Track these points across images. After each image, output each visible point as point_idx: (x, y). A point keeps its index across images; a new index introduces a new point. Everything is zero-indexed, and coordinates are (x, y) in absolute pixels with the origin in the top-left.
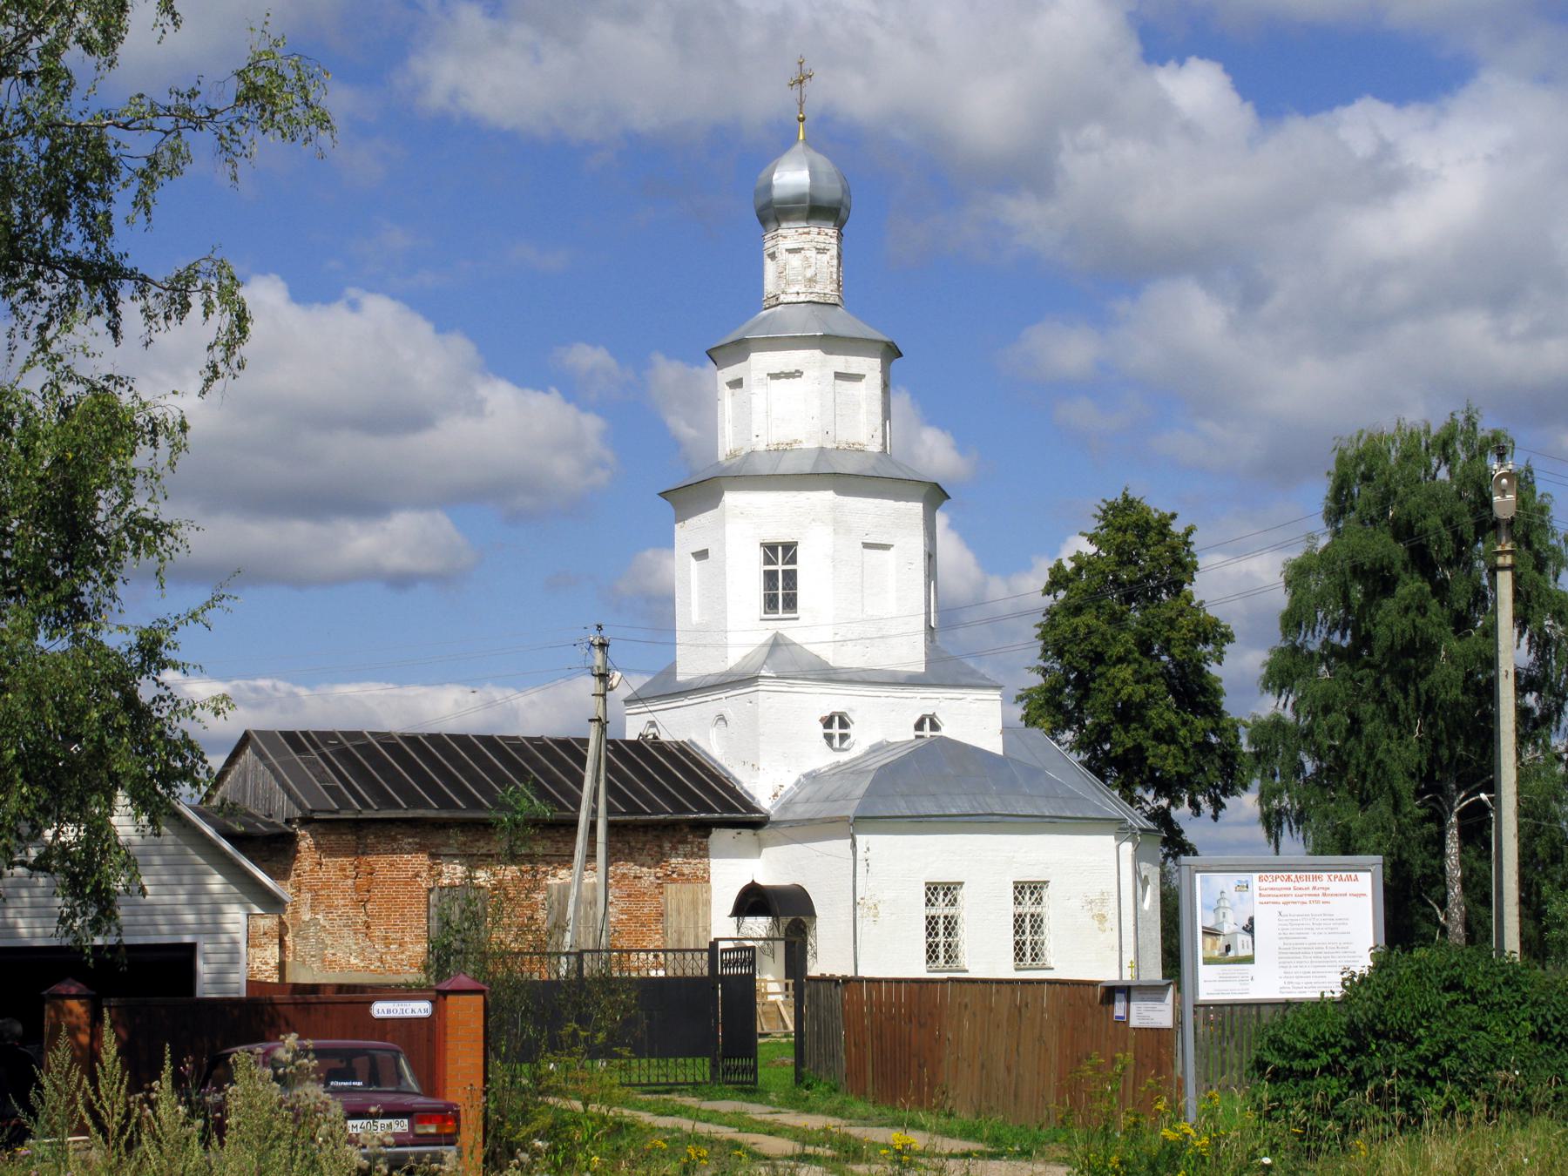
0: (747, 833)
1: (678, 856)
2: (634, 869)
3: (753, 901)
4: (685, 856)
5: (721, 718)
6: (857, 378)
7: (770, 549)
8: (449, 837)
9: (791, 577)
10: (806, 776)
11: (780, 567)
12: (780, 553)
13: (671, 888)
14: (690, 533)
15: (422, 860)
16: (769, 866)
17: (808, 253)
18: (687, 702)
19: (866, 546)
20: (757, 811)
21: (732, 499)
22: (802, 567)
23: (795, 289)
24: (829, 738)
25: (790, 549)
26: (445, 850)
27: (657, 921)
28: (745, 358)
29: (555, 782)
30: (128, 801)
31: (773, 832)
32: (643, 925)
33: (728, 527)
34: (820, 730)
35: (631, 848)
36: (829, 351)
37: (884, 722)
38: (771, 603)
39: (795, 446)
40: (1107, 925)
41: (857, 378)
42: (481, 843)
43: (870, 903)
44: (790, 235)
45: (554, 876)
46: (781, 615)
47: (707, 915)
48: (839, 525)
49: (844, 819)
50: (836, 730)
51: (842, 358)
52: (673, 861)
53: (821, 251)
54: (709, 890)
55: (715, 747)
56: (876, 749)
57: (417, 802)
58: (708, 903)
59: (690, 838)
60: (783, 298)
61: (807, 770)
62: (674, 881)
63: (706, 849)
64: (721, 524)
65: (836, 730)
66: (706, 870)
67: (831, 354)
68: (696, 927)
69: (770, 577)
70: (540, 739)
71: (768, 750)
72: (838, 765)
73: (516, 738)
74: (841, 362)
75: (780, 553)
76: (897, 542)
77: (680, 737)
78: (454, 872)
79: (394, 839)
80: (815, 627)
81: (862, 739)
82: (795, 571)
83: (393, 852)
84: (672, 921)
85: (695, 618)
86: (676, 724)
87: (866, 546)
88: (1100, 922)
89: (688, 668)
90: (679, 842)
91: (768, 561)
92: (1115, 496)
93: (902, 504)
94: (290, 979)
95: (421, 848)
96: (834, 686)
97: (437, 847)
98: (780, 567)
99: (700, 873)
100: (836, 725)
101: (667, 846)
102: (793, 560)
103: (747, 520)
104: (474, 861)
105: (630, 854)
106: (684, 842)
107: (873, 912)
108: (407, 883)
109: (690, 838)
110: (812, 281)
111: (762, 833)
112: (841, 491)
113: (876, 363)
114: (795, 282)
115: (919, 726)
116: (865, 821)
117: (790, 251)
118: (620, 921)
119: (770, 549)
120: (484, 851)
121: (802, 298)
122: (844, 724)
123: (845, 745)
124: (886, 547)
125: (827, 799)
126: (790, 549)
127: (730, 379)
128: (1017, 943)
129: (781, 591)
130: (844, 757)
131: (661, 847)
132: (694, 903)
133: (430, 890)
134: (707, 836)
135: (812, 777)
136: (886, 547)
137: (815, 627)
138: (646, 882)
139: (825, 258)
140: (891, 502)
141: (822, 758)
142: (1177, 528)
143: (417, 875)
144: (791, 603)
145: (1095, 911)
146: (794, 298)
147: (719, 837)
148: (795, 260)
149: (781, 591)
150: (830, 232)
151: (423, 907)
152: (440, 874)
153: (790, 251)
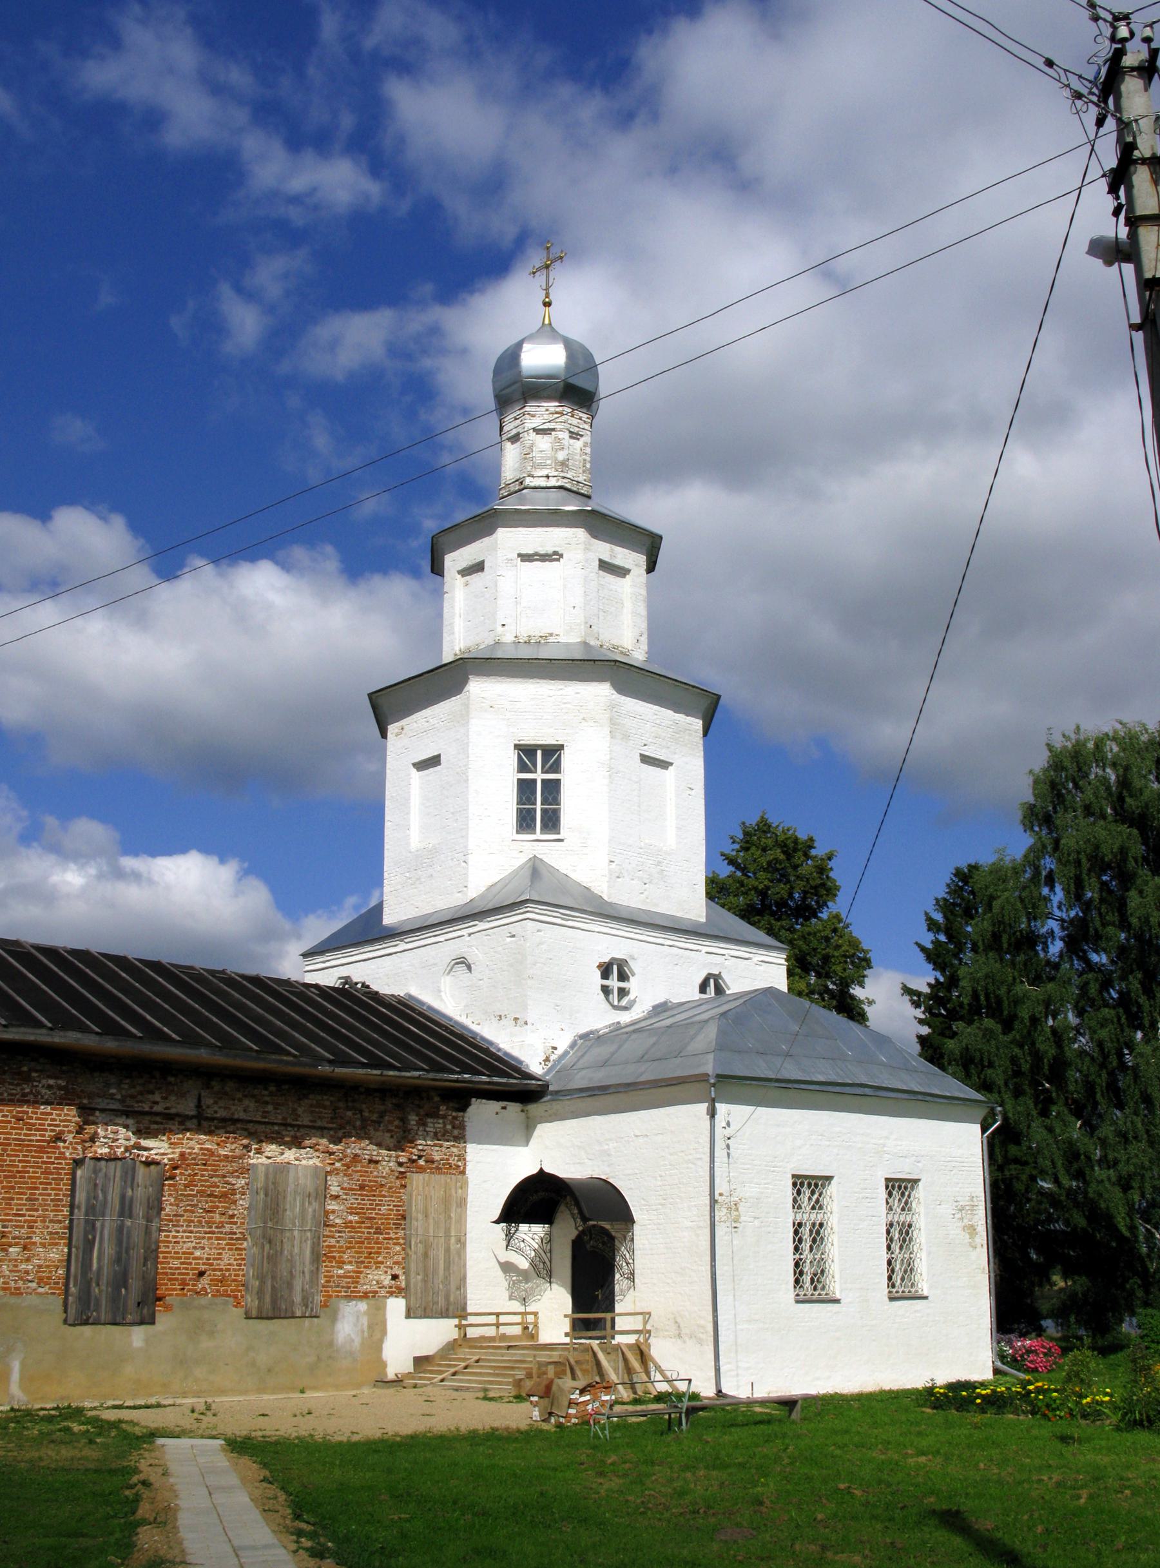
0: (514, 1108)
3: (536, 1199)
4: (436, 1136)
5: (463, 962)
6: (622, 572)
7: (526, 753)
8: (108, 1085)
9: (552, 789)
10: (584, 1037)
11: (539, 776)
12: (539, 761)
13: (417, 1181)
14: (410, 737)
15: (69, 1115)
16: (563, 1148)
17: (561, 435)
18: (403, 946)
19: (646, 760)
20: (530, 1076)
21: (478, 688)
22: (570, 776)
23: (545, 472)
24: (606, 990)
25: (552, 754)
26: (102, 1103)
28: (490, 531)
30: (250, 1104)
31: (556, 1106)
32: (378, 1231)
33: (473, 722)
34: (597, 980)
35: (363, 1119)
36: (595, 533)
37: (668, 976)
38: (525, 822)
39: (551, 639)
41: (622, 572)
42: (157, 1097)
44: (541, 412)
45: (259, 1152)
46: (538, 835)
47: (462, 1220)
48: (617, 730)
49: (703, 1078)
50: (614, 983)
53: (575, 436)
54: (464, 1185)
55: (449, 1000)
56: (661, 1009)
57: (64, 1022)
58: (462, 1203)
59: (443, 1109)
60: (528, 481)
61: (583, 1030)
62: (421, 1170)
63: (462, 1127)
64: (464, 718)
65: (614, 983)
66: (462, 1157)
68: (447, 1236)
69: (525, 789)
70: (223, 972)
71: (529, 1004)
72: (617, 1027)
73: (192, 968)
74: (605, 550)
75: (539, 761)
77: (399, 991)
78: (114, 1138)
79: (27, 1079)
80: (581, 853)
81: (646, 993)
82: (559, 780)
83: (23, 1101)
84: (417, 1223)
85: (415, 840)
86: (384, 972)
87: (646, 760)
89: (390, 918)
90: (428, 1115)
91: (523, 767)
92: (752, 821)
93: (681, 717)
94: (703, 1107)
95: (64, 1098)
97: (90, 1096)
98: (539, 776)
99: (453, 1161)
100: (614, 970)
101: (413, 1119)
102: (556, 767)
103: (491, 722)
104: (150, 1124)
105: (363, 1127)
106: (434, 1115)
108: (41, 1150)
109: (443, 1109)
110: (564, 464)
111: (533, 1108)
112: (622, 688)
114: (542, 466)
115: (703, 988)
116: (727, 1086)
117: (537, 431)
118: (348, 1224)
119: (526, 753)
120: (222, 1113)
121: (553, 482)
122: (623, 977)
123: (624, 1002)
125: (641, 1059)
126: (552, 754)
127: (464, 564)
129: (539, 802)
130: (625, 1018)
131: (404, 1120)
132: (446, 1201)
133: (78, 1163)
134: (464, 1108)
135: (588, 1039)
136: (664, 765)
137: (581, 853)
139: (578, 444)
140: (670, 712)
141: (599, 1016)
142: (818, 851)
143: (58, 1138)
144: (552, 822)
146: (543, 482)
147: (481, 1111)
148: (543, 444)
149: (539, 802)
150: (584, 416)
151: (65, 1188)
152: (93, 1139)
153: (537, 431)
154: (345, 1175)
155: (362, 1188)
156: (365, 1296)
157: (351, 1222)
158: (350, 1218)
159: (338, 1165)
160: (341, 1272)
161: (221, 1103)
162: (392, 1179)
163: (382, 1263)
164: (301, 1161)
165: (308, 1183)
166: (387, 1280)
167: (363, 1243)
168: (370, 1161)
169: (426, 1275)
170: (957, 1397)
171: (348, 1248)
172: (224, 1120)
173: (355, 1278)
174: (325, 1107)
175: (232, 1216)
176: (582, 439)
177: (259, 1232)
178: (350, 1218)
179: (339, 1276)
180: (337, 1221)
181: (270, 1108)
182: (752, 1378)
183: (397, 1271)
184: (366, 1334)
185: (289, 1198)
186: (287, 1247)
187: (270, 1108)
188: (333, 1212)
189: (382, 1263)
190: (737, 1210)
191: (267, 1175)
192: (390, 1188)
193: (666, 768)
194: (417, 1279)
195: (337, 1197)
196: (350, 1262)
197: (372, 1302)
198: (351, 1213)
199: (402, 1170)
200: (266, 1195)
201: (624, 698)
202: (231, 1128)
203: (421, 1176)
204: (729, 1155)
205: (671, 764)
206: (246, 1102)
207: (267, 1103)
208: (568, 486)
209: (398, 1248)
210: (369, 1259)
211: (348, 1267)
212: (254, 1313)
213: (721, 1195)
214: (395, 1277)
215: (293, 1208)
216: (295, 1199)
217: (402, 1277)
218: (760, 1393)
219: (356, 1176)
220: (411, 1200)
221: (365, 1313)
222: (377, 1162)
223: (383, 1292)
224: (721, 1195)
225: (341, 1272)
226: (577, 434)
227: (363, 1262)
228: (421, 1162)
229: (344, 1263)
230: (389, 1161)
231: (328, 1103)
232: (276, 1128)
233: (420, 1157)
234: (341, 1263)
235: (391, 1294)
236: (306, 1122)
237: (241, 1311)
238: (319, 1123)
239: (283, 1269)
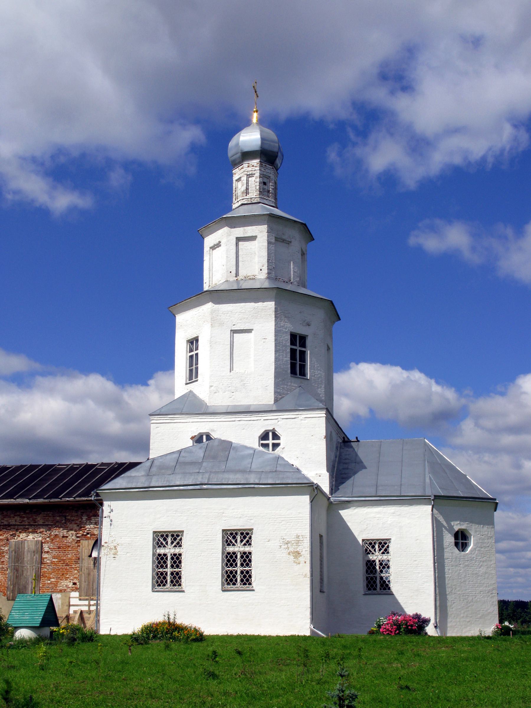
1: (91, 523)
2: (64, 532)
6: (253, 238)
27: (77, 563)
29: (37, 486)
30: (18, 518)
32: (67, 565)
40: (301, 559)
41: (253, 238)
43: (112, 546)
51: (242, 229)
52: (88, 526)
61: (319, 484)
67: (235, 227)
76: (255, 327)
88: (296, 557)
93: (260, 304)
96: (201, 417)
98: (298, 348)
107: (113, 551)
113: (264, 228)
118: (52, 562)
120: (6, 523)
124: (249, 331)
128: (178, 566)
136: (249, 331)
138: (70, 539)
140: (252, 304)
145: (291, 549)
154: (51, 543)
155: (59, 548)
156: (61, 591)
157: (54, 562)
158: (54, 560)
159: (48, 539)
160: (49, 582)
161: (6, 519)
162: (73, 543)
163: (68, 578)
164: (30, 539)
165: (33, 547)
166: (71, 585)
167: (59, 570)
168: (63, 537)
169: (89, 583)
170: (305, 638)
171: (52, 572)
172: (5, 525)
173: (56, 584)
174: (50, 517)
175: (3, 562)
176: (255, 176)
177: (13, 567)
178: (54, 560)
179: (48, 584)
180: (48, 562)
181: (25, 519)
182: (111, 626)
183: (75, 581)
184: (60, 607)
185: (26, 553)
186: (25, 572)
187: (25, 519)
188: (46, 558)
189: (68, 578)
190: (116, 549)
191: (15, 545)
192: (73, 547)
193: (251, 332)
194: (84, 585)
195: (48, 552)
196: (53, 578)
197: (63, 594)
198: (54, 558)
199: (78, 539)
200: (15, 553)
201: (221, 305)
202: (9, 528)
203: (87, 542)
204: (111, 524)
205: (252, 330)
206: (16, 518)
207: (24, 517)
208: (245, 202)
209: (76, 572)
210: (63, 576)
211: (53, 580)
212: (11, 598)
213: (106, 543)
214: (75, 584)
215: (27, 557)
216: (28, 554)
217: (78, 584)
218: (120, 632)
219: (56, 543)
220: (82, 551)
221: (60, 598)
222: (67, 537)
223: (69, 590)
224: (106, 543)
225: (49, 582)
226: (252, 174)
227: (59, 578)
228: (89, 536)
229: (51, 578)
230: (72, 535)
231: (50, 515)
232: (27, 527)
233: (88, 534)
234: (49, 579)
235: (73, 590)
236: (41, 523)
237: (6, 597)
238: (47, 523)
239: (22, 582)
